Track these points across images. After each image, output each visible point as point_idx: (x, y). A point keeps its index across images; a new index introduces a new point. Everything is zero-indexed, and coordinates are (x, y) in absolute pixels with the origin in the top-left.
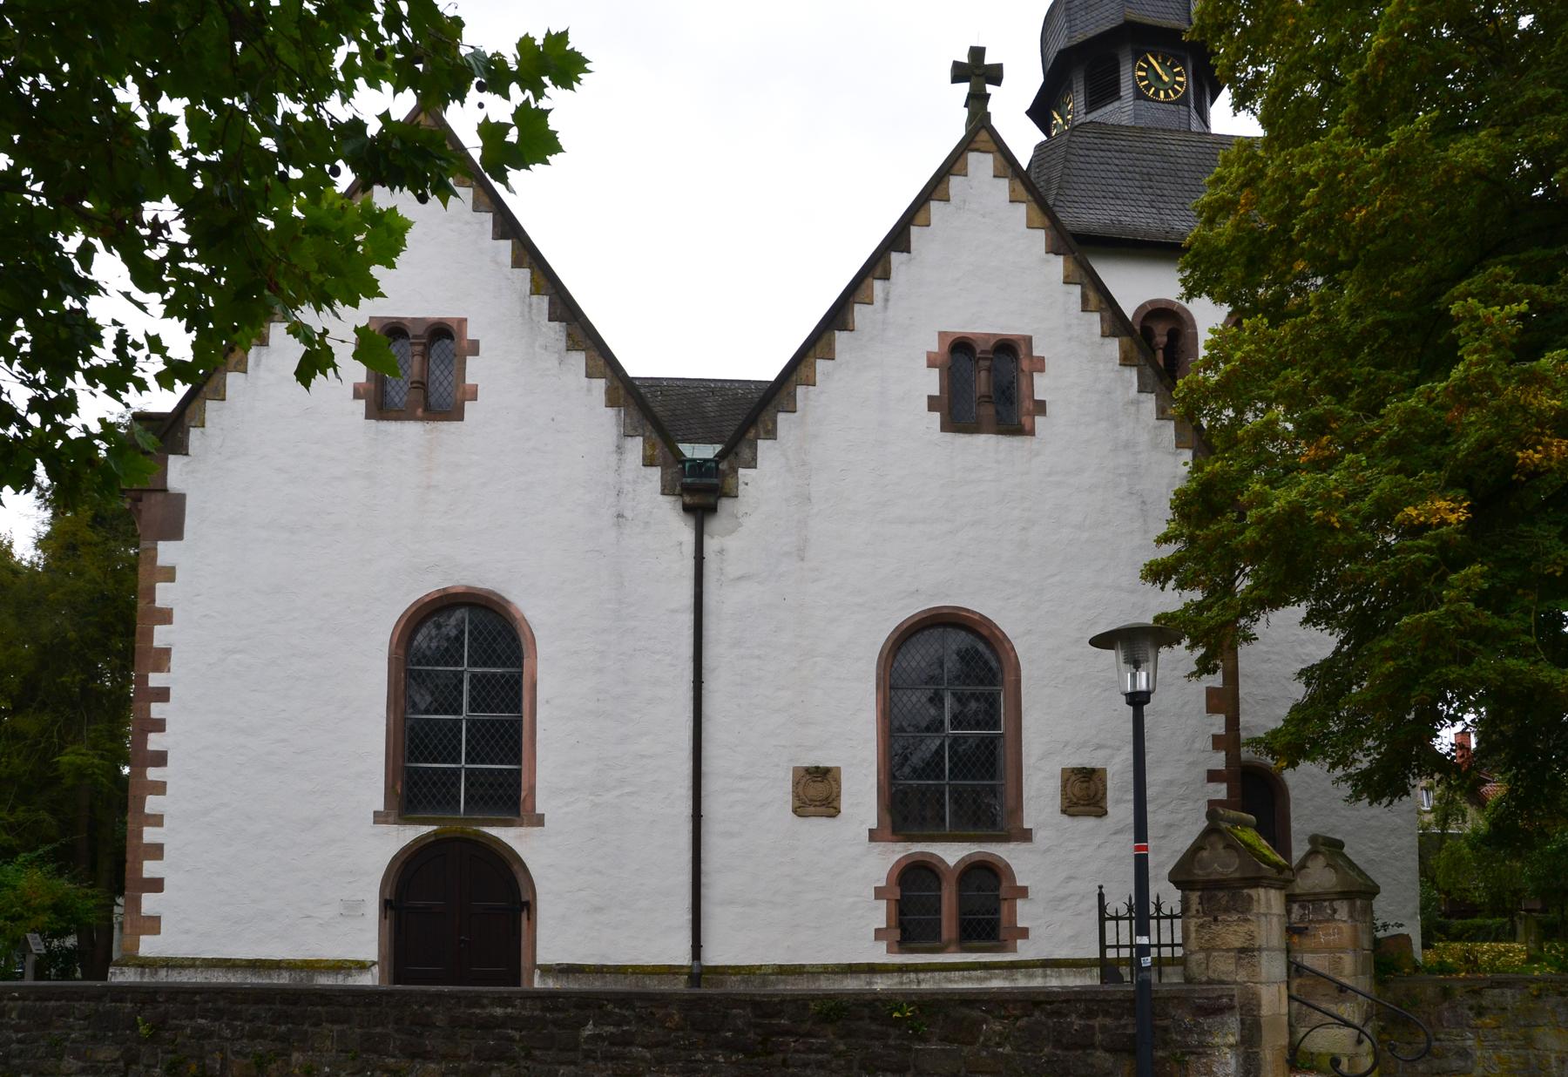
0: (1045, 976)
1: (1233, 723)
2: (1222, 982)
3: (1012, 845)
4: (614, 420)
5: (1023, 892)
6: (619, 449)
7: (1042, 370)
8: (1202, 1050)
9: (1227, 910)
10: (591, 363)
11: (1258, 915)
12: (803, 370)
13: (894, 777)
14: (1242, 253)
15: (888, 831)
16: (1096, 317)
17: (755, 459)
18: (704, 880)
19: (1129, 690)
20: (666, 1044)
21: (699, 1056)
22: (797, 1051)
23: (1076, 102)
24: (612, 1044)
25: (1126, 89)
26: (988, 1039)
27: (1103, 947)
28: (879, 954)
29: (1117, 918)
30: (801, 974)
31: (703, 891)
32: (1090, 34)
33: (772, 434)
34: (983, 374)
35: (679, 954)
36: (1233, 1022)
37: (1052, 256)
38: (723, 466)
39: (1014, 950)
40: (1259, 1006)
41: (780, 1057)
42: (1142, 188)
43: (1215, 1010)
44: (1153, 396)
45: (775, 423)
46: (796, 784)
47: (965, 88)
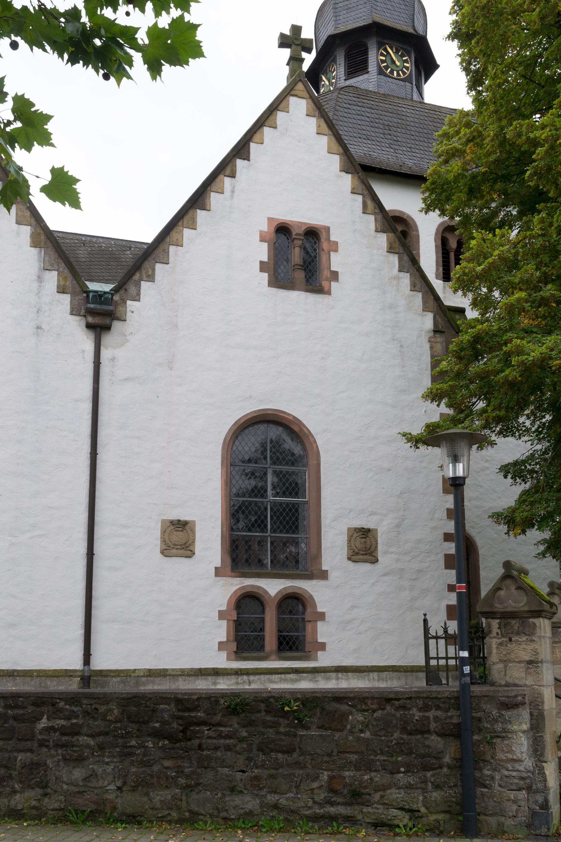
0: (338, 679)
1: (459, 501)
2: (516, 685)
3: (314, 582)
4: (36, 257)
5: (322, 616)
6: (40, 279)
7: (336, 251)
8: (504, 735)
9: (518, 634)
10: (20, 214)
11: (540, 637)
12: (174, 235)
13: (232, 529)
14: (465, 185)
15: (229, 569)
16: (372, 218)
17: (139, 294)
18: (94, 603)
19: (451, 475)
20: (107, 734)
21: (133, 743)
22: (209, 737)
23: (339, 70)
24: (63, 734)
25: (372, 66)
26: (353, 727)
27: (428, 658)
28: (221, 661)
29: (437, 638)
30: (165, 676)
31: (94, 612)
32: (349, 27)
33: (151, 278)
34: (297, 250)
35: (75, 662)
36: (525, 713)
37: (344, 174)
38: (116, 298)
39: (316, 659)
40: (543, 702)
41: (196, 742)
42: (384, 134)
43: (511, 705)
44: (408, 275)
45: (154, 270)
46: (163, 532)
47: (287, 53)
